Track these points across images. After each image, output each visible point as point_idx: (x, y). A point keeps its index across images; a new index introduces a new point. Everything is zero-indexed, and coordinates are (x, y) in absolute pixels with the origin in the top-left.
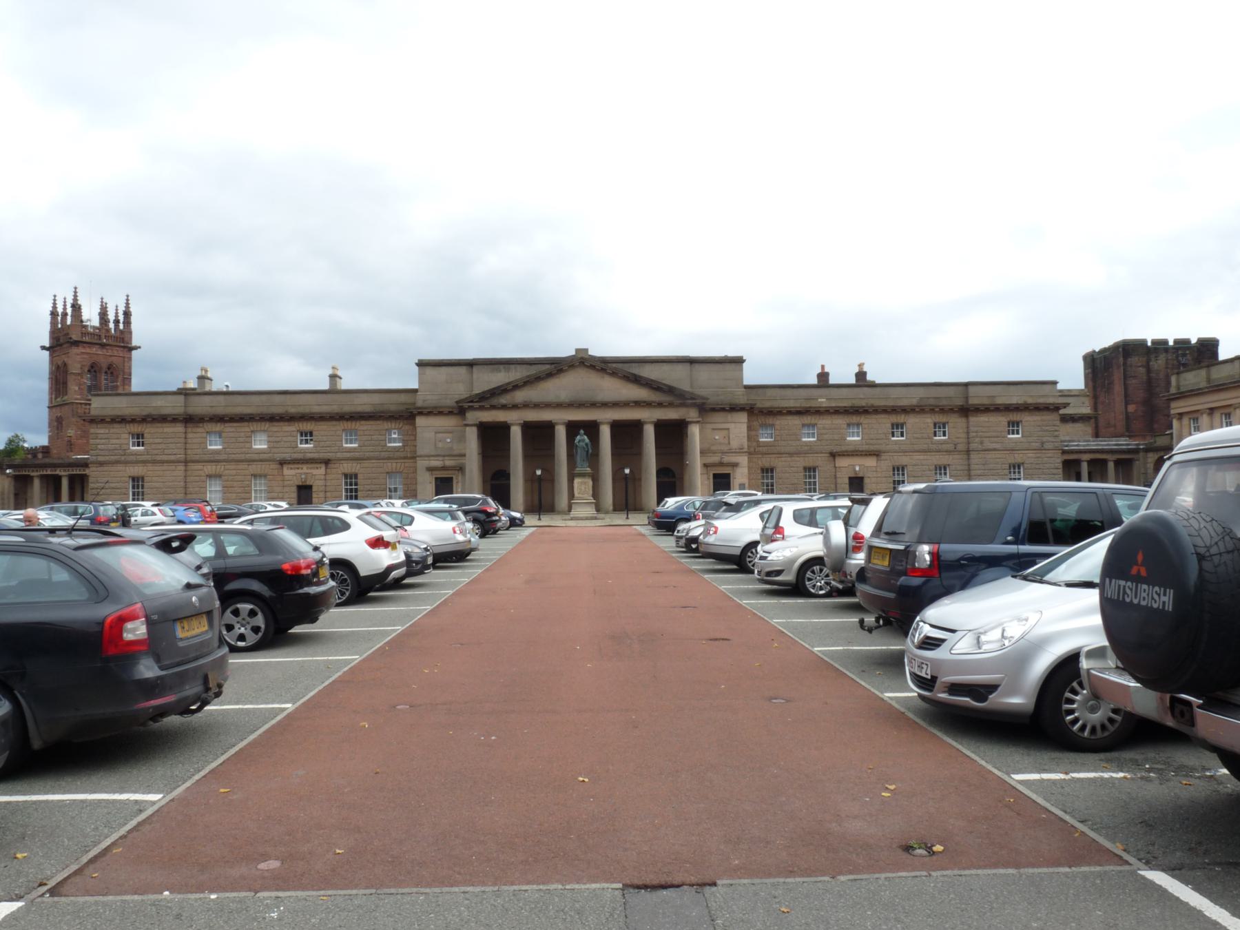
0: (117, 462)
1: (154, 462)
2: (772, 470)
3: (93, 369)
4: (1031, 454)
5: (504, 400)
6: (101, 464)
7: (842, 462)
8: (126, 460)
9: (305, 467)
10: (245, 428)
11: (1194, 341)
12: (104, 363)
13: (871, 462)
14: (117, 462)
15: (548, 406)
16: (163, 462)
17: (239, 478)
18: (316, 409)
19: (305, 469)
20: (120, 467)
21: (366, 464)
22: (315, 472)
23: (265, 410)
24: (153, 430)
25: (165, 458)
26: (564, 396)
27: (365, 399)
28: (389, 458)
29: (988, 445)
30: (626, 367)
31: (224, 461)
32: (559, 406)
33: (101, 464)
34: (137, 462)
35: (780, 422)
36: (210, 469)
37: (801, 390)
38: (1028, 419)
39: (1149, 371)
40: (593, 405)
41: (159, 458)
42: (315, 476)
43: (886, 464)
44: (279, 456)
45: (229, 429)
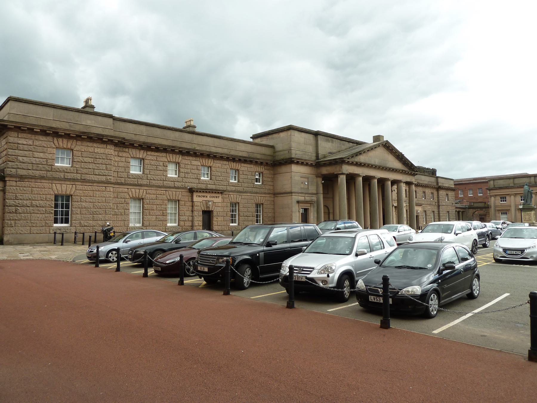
0: (42, 178)
1: (84, 181)
2: (448, 212)
6: (22, 178)
8: (53, 176)
9: (208, 195)
10: (163, 157)
11: (385, 139)
14: (42, 178)
16: (93, 182)
17: (158, 202)
18: (214, 150)
19: (208, 197)
20: (46, 184)
21: (245, 196)
22: (215, 200)
23: (142, 139)
24: (83, 148)
25: (96, 178)
28: (256, 193)
30: (517, 181)
31: (146, 186)
33: (22, 178)
34: (66, 180)
36: (135, 191)
37: (205, 138)
41: (88, 177)
42: (217, 204)
44: (189, 185)
45: (150, 156)
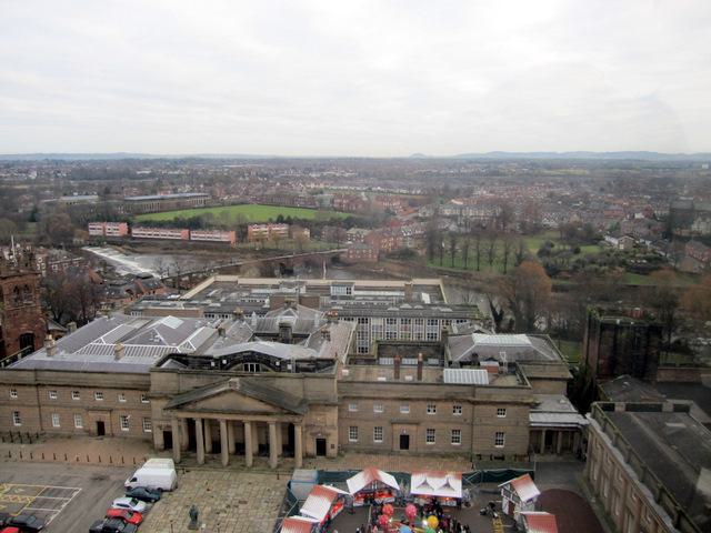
3: (17, 290)
4: (509, 428)
5: (190, 407)
7: (397, 427)
12: (22, 285)
13: (414, 428)
15: (217, 412)
19: (100, 414)
26: (224, 406)
27: (127, 377)
29: (484, 422)
32: (223, 412)
35: (362, 402)
38: (510, 409)
39: (615, 338)
40: (243, 413)
43: (423, 428)
